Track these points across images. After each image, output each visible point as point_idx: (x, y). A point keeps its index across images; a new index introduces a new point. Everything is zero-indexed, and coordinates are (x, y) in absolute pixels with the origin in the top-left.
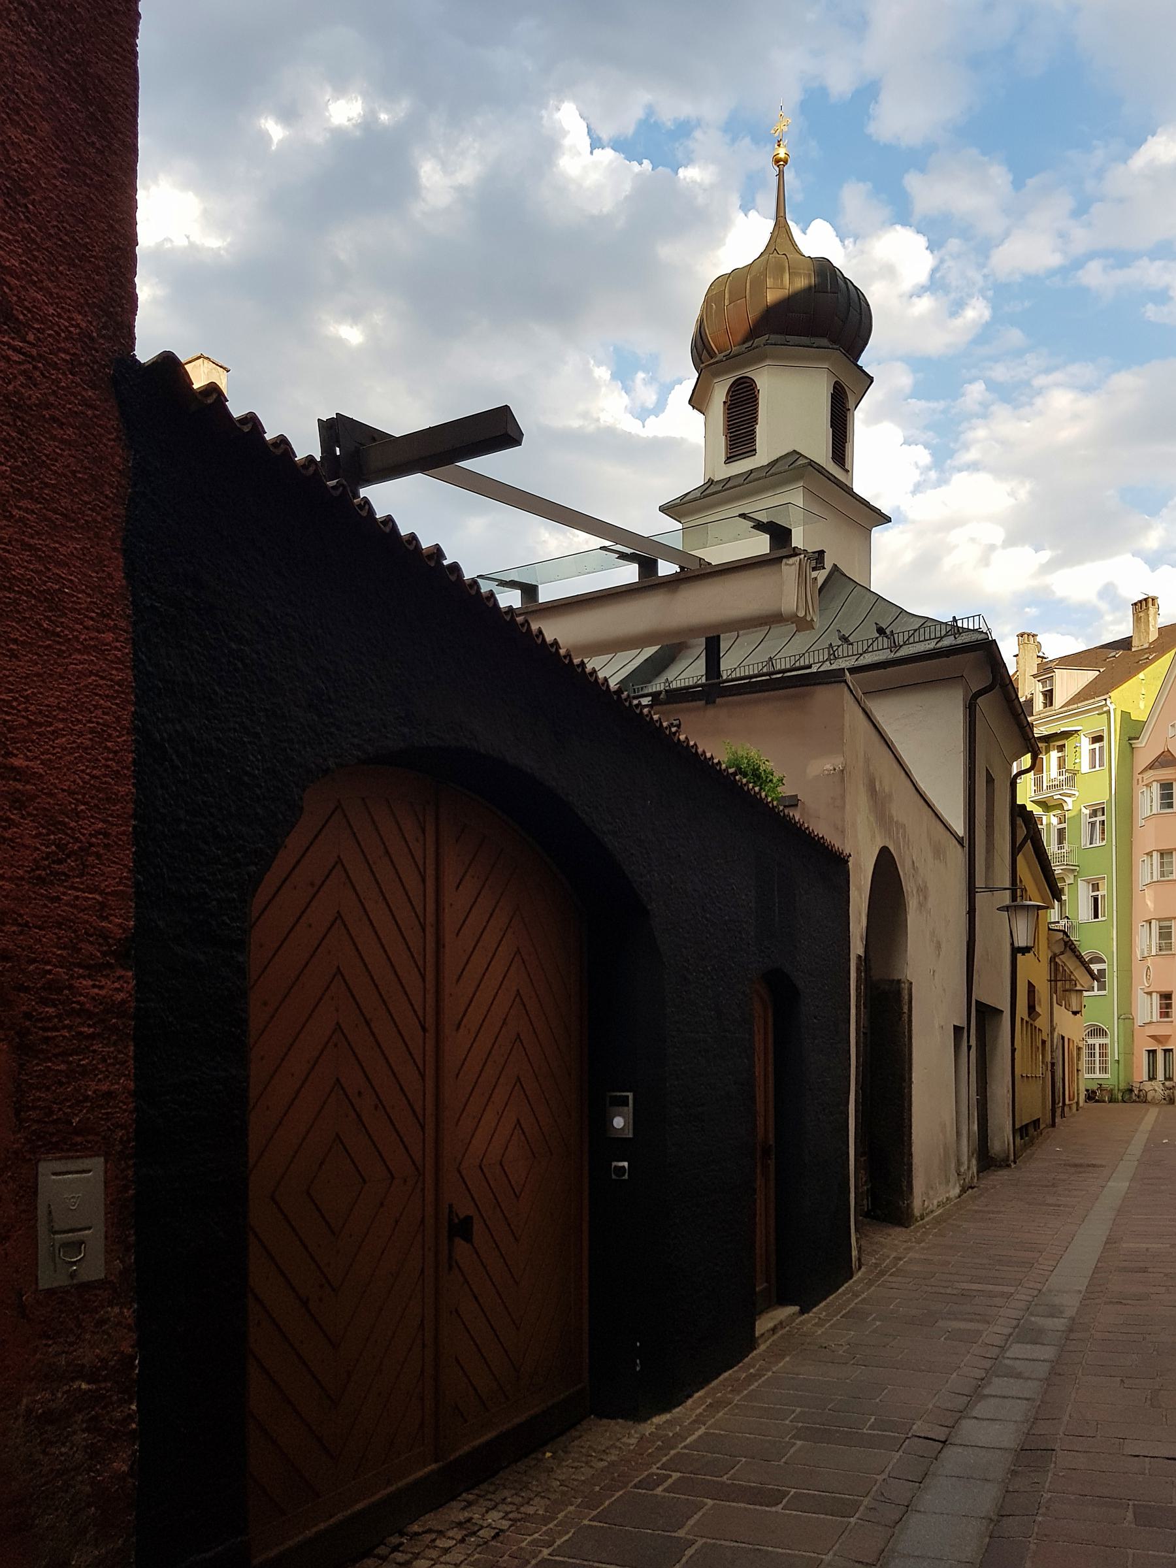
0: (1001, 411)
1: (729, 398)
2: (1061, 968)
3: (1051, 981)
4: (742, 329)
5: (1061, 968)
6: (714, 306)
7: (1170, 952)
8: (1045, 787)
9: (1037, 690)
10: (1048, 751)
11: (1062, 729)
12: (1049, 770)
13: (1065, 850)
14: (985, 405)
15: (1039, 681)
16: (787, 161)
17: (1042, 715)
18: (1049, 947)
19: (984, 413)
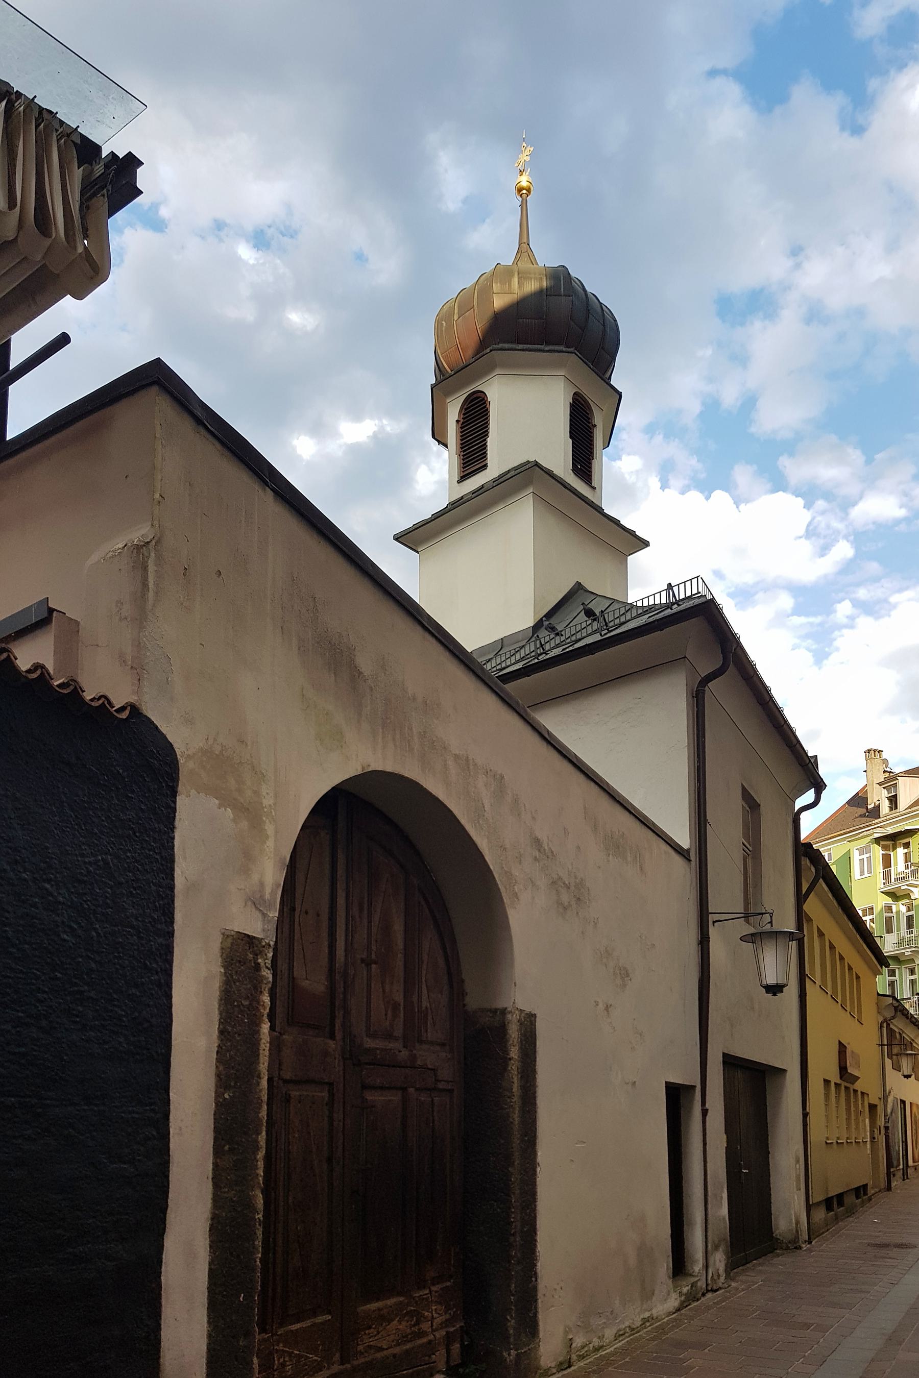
0: (864, 621)
1: (462, 416)
2: (898, 1035)
3: (882, 1045)
4: (472, 342)
5: (898, 1035)
6: (444, 325)
7: (879, 820)
8: (893, 880)
9: (883, 796)
10: (894, 848)
11: (906, 828)
12: (896, 864)
13: (913, 935)
14: (852, 618)
15: (884, 788)
16: (530, 189)
17: (888, 817)
18: (879, 1012)
19: (851, 624)
